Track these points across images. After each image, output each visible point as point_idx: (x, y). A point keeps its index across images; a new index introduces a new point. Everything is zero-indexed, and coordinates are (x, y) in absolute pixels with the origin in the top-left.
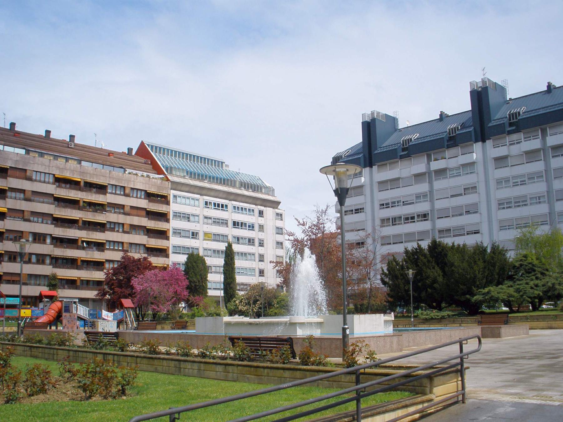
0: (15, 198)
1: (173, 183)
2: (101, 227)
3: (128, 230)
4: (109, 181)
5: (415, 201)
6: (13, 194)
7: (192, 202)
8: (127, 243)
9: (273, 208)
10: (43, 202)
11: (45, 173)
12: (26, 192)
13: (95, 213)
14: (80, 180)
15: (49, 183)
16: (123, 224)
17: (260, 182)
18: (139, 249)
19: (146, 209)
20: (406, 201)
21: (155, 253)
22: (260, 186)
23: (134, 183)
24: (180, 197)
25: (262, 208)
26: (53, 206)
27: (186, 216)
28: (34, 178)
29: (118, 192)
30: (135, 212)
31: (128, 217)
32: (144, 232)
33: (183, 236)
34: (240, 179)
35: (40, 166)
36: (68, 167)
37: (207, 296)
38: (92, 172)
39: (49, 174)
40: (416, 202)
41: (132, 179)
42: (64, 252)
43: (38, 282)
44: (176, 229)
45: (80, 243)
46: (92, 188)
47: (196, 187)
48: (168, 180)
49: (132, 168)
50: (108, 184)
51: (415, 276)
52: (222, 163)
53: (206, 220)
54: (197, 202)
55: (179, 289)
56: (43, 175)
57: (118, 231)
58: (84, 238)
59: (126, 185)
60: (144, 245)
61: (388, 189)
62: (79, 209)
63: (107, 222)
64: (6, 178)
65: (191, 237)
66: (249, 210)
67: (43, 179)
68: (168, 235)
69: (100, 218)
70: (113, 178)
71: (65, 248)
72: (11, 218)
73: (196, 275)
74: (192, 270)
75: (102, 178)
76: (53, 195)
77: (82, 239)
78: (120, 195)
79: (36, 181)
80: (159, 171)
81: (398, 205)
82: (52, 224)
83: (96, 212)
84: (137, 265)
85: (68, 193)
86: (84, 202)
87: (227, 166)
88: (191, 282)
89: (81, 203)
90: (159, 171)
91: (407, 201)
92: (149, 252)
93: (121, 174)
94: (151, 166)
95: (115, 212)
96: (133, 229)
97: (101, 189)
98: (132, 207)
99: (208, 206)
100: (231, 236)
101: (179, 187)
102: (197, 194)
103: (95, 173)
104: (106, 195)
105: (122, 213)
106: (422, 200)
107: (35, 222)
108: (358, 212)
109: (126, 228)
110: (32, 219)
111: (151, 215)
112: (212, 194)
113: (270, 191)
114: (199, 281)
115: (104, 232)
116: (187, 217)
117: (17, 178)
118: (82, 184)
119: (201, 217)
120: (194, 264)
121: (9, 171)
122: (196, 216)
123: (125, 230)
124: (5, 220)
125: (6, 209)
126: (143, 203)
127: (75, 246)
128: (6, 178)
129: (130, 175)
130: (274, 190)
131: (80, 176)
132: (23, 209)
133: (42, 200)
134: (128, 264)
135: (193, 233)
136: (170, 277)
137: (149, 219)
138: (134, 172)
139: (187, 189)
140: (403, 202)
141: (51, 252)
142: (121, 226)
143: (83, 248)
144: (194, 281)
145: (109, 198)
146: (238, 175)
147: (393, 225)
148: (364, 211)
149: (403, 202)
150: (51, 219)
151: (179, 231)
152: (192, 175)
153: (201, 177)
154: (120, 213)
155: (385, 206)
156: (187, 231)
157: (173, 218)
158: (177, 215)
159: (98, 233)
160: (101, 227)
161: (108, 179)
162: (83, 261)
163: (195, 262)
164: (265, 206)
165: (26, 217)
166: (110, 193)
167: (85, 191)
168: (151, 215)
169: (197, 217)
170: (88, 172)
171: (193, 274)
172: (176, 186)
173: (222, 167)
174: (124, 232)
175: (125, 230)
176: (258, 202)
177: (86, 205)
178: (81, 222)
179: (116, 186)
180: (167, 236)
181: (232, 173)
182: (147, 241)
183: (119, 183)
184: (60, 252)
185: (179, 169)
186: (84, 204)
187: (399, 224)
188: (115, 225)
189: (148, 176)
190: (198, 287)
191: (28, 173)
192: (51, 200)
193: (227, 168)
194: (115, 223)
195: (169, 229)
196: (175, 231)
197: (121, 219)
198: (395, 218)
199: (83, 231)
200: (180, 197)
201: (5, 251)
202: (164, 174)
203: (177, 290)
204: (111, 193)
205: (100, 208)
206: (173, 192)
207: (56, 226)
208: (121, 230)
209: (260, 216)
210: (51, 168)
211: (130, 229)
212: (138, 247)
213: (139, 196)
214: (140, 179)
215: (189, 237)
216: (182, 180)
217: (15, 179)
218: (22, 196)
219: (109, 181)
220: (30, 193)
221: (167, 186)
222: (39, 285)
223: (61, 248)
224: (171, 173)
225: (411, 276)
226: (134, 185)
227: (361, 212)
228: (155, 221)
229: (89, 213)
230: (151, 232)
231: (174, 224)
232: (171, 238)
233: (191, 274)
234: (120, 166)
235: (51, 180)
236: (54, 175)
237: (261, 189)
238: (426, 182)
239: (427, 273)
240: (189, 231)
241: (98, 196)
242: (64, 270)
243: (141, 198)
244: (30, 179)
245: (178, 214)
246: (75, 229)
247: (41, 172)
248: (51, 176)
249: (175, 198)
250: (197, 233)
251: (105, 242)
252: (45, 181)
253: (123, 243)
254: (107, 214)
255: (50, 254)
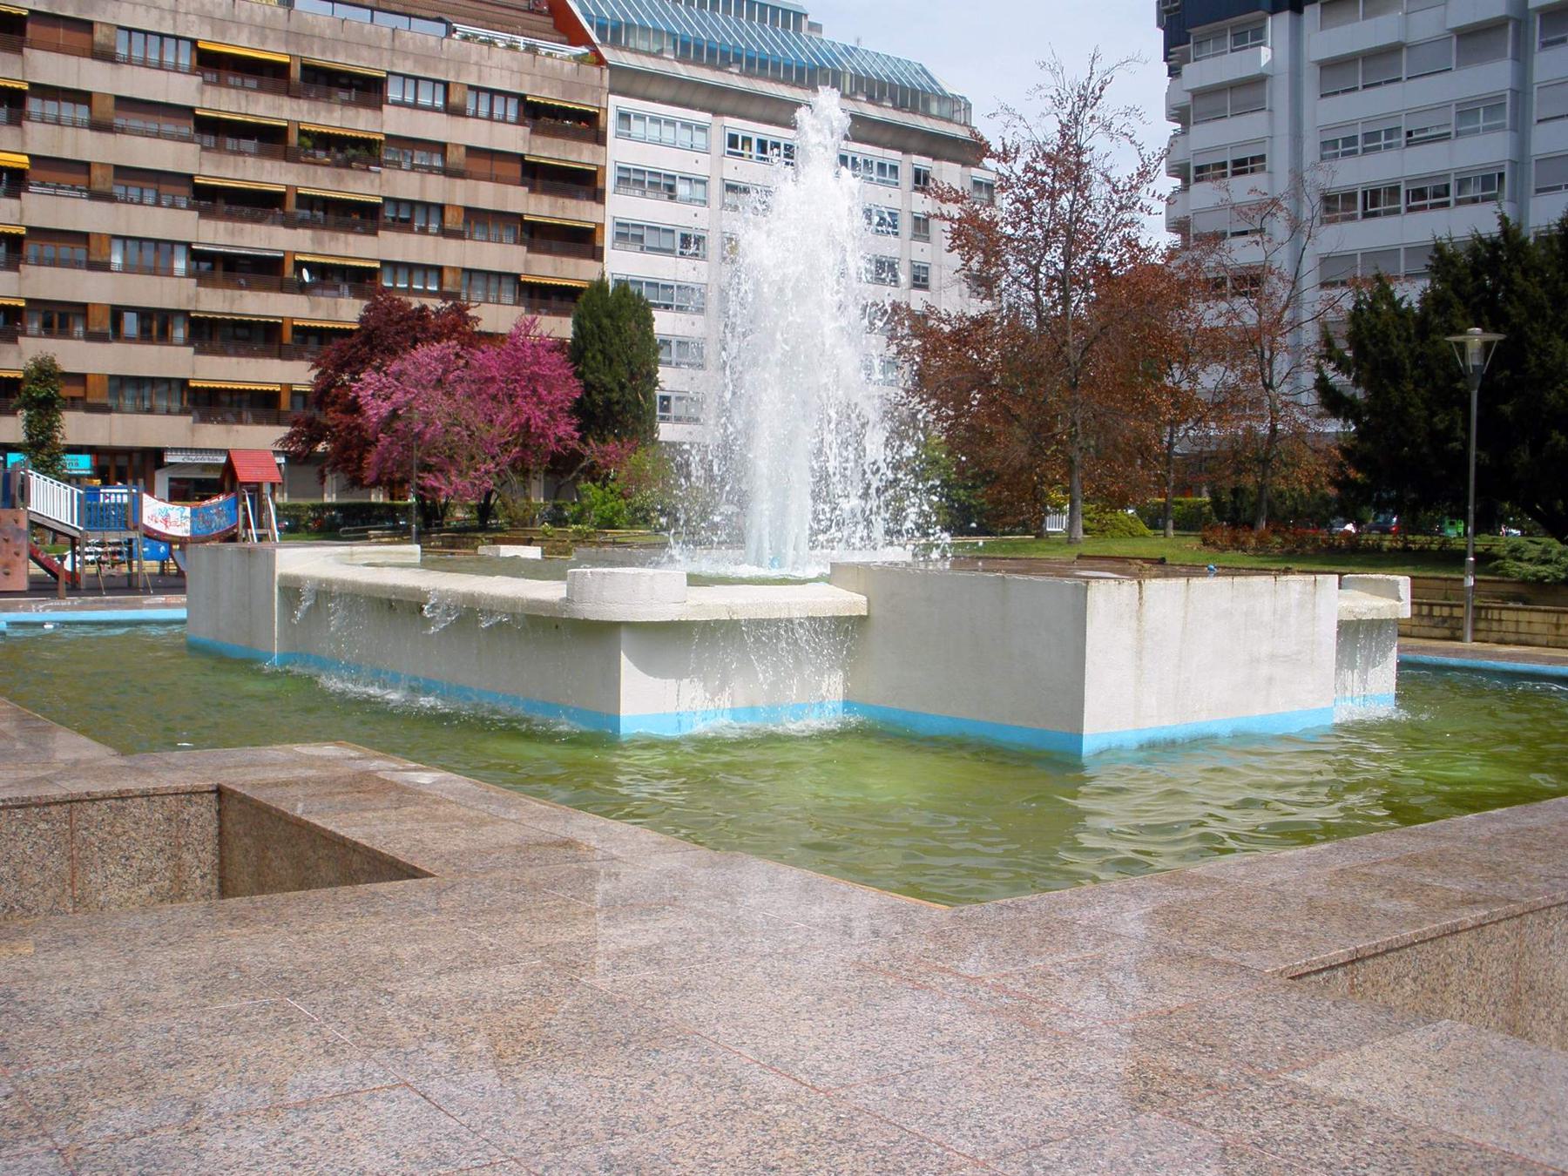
0: (58, 122)
1: (616, 70)
2: (364, 216)
3: (460, 227)
4: (392, 64)
5: (1452, 129)
6: (51, 108)
7: (684, 136)
8: (454, 269)
9: (964, 164)
10: (158, 135)
11: (162, 36)
12: (95, 101)
13: (344, 171)
14: (287, 60)
15: (176, 69)
16: (441, 208)
17: (924, 81)
18: (499, 290)
19: (522, 156)
20: (1418, 131)
21: (554, 302)
22: (924, 92)
23: (480, 71)
24: (641, 117)
25: (924, 162)
26: (192, 149)
27: (663, 181)
28: (122, 51)
29: (424, 100)
30: (483, 165)
31: (459, 183)
32: (516, 233)
33: (649, 248)
34: (854, 69)
35: (141, 10)
36: (243, 16)
37: (655, 441)
38: (328, 33)
39: (177, 38)
40: (1458, 134)
41: (474, 58)
42: (233, 301)
43: (147, 404)
44: (627, 225)
45: (289, 270)
46: (334, 90)
47: (699, 86)
48: (600, 61)
49: (480, 22)
50: (388, 73)
51: (1498, 356)
52: (799, 16)
53: (730, 198)
54: (700, 139)
55: (538, 417)
56: (154, 42)
57: (424, 231)
58: (303, 253)
59: (451, 79)
60: (516, 277)
61: (1356, 89)
62: (286, 159)
63: (385, 199)
64: (20, 52)
65: (678, 250)
66: (882, 166)
67: (137, 54)
68: (598, 244)
69: (361, 186)
70: (406, 54)
71: (241, 287)
72: (45, 190)
73: (611, 361)
74: (598, 346)
75: (365, 53)
76: (192, 109)
77: (298, 258)
78: (433, 109)
79: (129, 61)
80: (578, 36)
81: (1388, 146)
82: (190, 207)
83: (347, 165)
84: (412, 328)
85: (243, 103)
86: (303, 133)
87: (815, 27)
88: (593, 387)
89: (293, 139)
90: (578, 36)
91: (1425, 130)
92: (537, 301)
93: (432, 41)
94: (551, 20)
95: (413, 168)
96: (477, 223)
97: (368, 89)
98: (472, 151)
99: (739, 150)
100: (718, 182)
101: (639, 87)
102: (702, 109)
103: (342, 36)
104: (380, 109)
105: (438, 169)
106: (1481, 124)
107: (131, 202)
108: (1244, 172)
109: (453, 220)
110: (119, 191)
111: (539, 176)
112: (755, 109)
113: (957, 106)
114: (622, 387)
115: (373, 232)
116: (665, 186)
117: (58, 49)
118: (296, 73)
119: (716, 188)
120: (606, 322)
121: (29, 27)
122: (698, 181)
123: (448, 225)
124: (23, 195)
125: (25, 159)
126: (513, 138)
127: (275, 279)
128: (20, 52)
129: (466, 44)
130: (968, 106)
131: (287, 44)
132: (87, 159)
133: (153, 127)
134: (377, 328)
135: (685, 239)
136: (508, 369)
137: (533, 190)
138: (483, 33)
139: (668, 92)
140: (1409, 134)
141: (189, 299)
142: (435, 215)
143: (302, 288)
144: (603, 385)
145: (392, 121)
146: (851, 55)
147: (1366, 215)
148: (1263, 168)
149: (1409, 134)
150: (187, 190)
151: (638, 232)
152: (688, 50)
153: (719, 57)
154: (431, 170)
155: (1341, 149)
156: (665, 231)
157: (617, 186)
158: (632, 179)
159: (352, 238)
160: (364, 216)
161: (387, 55)
162: (297, 330)
163: (610, 316)
164: (935, 158)
165: (97, 187)
166: (395, 104)
167: (308, 98)
168: (539, 176)
169: (700, 187)
170: (317, 31)
171: (599, 357)
172: (629, 82)
173: (798, 28)
174: (445, 233)
175: (448, 225)
176: (913, 142)
177: (309, 143)
178: (291, 201)
179: (416, 79)
180: (594, 247)
181: (830, 51)
182: (527, 263)
183: (426, 69)
184: (217, 301)
185: (644, 28)
186: (304, 139)
187: (1388, 213)
188: (412, 211)
189: (531, 49)
190: (617, 408)
191: (100, 36)
192: (187, 128)
193: (814, 35)
194: (412, 204)
195: (602, 225)
196: (624, 230)
197: (435, 189)
198: (1375, 194)
199: (300, 231)
200: (641, 117)
201: (28, 301)
202: (587, 41)
203: (528, 419)
204: (401, 104)
205: (362, 153)
206: (616, 103)
207: (205, 214)
208: (434, 227)
209: (916, 189)
210: (180, 18)
211: (467, 221)
212: (493, 284)
213: (498, 112)
214: (500, 56)
215: (670, 252)
216: (650, 64)
217: (54, 55)
218: (82, 113)
219: (392, 64)
220: (111, 103)
221: (596, 82)
222: (150, 411)
223: (228, 287)
224: (615, 43)
225: (1474, 359)
226: (480, 78)
227: (1253, 170)
228: (552, 198)
229: (320, 170)
230: (539, 235)
231: (619, 206)
232: (608, 253)
233: (594, 358)
234: (439, 15)
235: (186, 59)
236: (194, 42)
237: (926, 103)
238: (1503, 56)
239: (1552, 355)
240: (673, 231)
241: (351, 112)
242: (234, 360)
243: (504, 121)
244: (106, 55)
245: (633, 176)
246: (273, 223)
247: (146, 33)
248: (185, 47)
249: (625, 122)
250: (699, 240)
251: (377, 265)
252: (145, 58)
253: (439, 270)
254: (385, 172)
255: (184, 307)
